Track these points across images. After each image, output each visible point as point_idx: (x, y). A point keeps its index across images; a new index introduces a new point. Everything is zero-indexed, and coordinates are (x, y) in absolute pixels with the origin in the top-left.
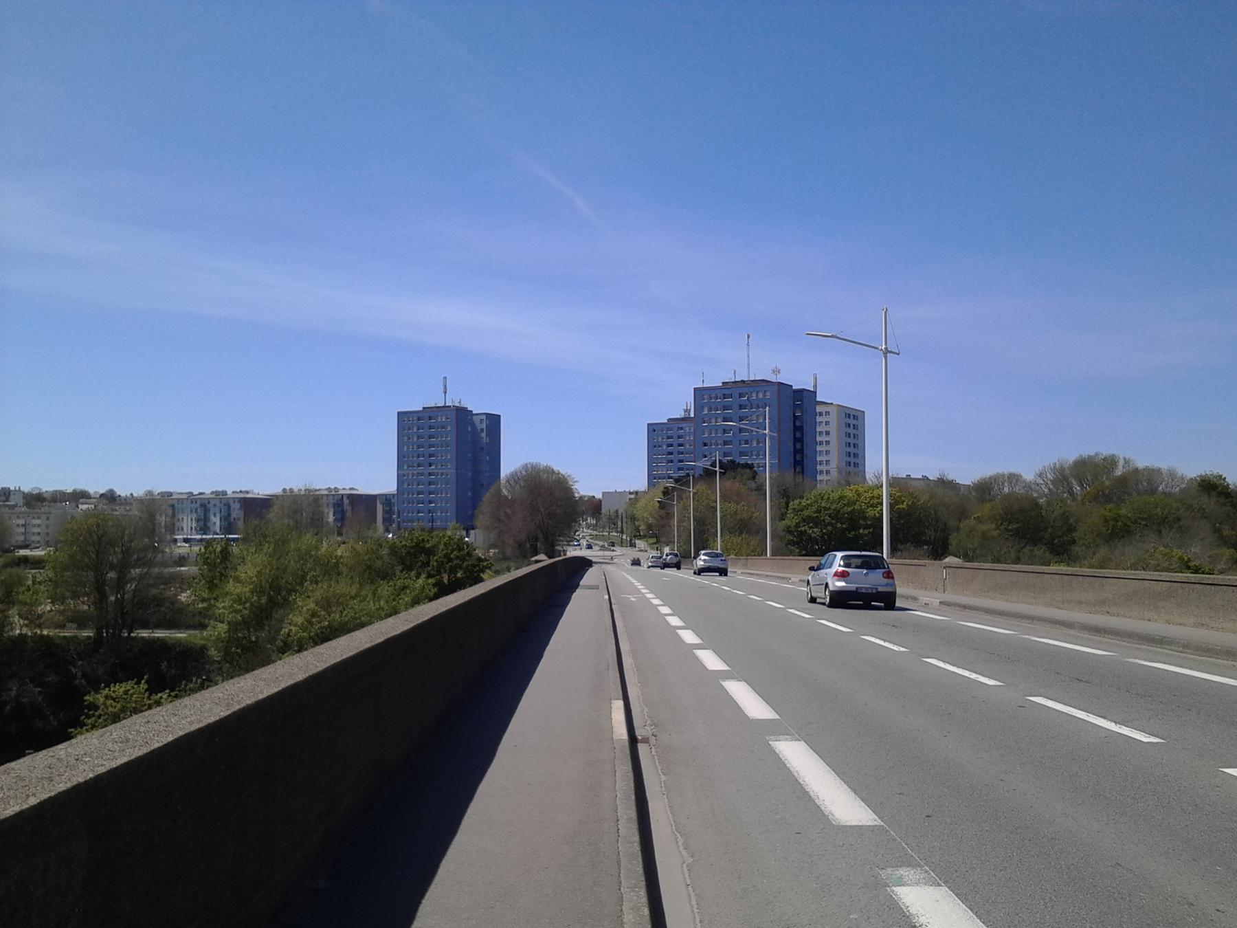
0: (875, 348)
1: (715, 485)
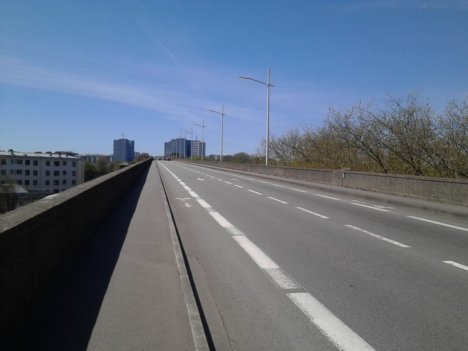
0: (265, 84)
1: (223, 158)
